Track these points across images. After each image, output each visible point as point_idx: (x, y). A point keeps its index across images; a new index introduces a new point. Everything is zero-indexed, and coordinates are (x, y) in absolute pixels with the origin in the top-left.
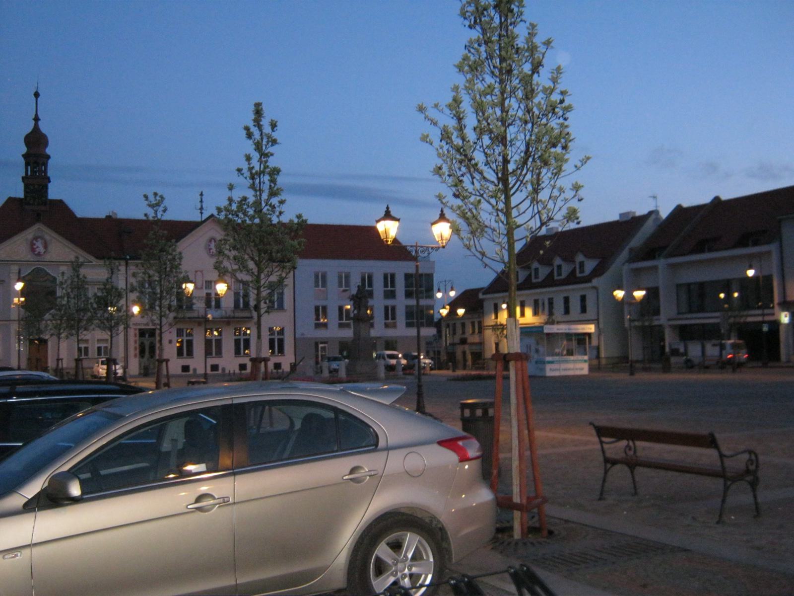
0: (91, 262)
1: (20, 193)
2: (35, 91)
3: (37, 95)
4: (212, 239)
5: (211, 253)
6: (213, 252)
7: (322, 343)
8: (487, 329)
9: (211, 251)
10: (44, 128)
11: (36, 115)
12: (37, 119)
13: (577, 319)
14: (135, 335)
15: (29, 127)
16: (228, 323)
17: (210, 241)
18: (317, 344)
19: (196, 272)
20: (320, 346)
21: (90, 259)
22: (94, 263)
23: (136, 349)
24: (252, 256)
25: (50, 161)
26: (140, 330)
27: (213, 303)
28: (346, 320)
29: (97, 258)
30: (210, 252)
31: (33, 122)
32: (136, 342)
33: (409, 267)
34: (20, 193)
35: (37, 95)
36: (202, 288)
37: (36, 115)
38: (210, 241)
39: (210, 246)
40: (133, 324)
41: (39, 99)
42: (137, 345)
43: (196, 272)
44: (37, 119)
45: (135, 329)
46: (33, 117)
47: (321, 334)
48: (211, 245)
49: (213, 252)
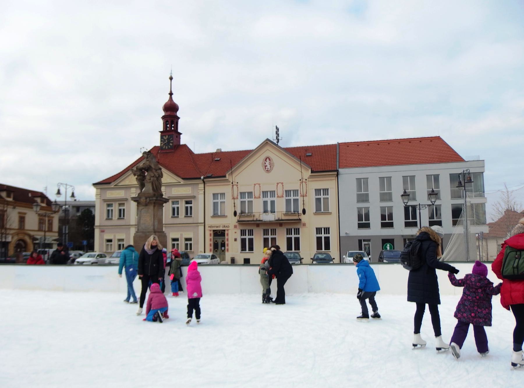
0: (180, 182)
1: (158, 144)
2: (169, 76)
3: (171, 79)
4: (267, 158)
5: (267, 169)
6: (268, 169)
7: (364, 240)
8: (406, 253)
9: (267, 167)
10: (176, 100)
11: (171, 91)
12: (171, 94)
13: (203, 195)
14: (211, 235)
15: (166, 99)
16: (281, 225)
17: (266, 160)
18: (360, 242)
19: (255, 185)
20: (363, 243)
21: (179, 181)
22: (182, 183)
23: (211, 245)
24: (504, 193)
25: (180, 120)
26: (214, 231)
27: (269, 209)
28: (388, 220)
29: (183, 179)
30: (266, 169)
31: (169, 96)
32: (211, 240)
33: (456, 168)
34: (158, 144)
35: (171, 79)
36: (260, 197)
37: (171, 91)
38: (266, 160)
39: (265, 163)
40: (209, 227)
41: (172, 81)
42: (212, 243)
43: (278, 184)
44: (171, 94)
45: (210, 230)
46: (169, 92)
47: (364, 233)
48: (266, 163)
49: (268, 169)
